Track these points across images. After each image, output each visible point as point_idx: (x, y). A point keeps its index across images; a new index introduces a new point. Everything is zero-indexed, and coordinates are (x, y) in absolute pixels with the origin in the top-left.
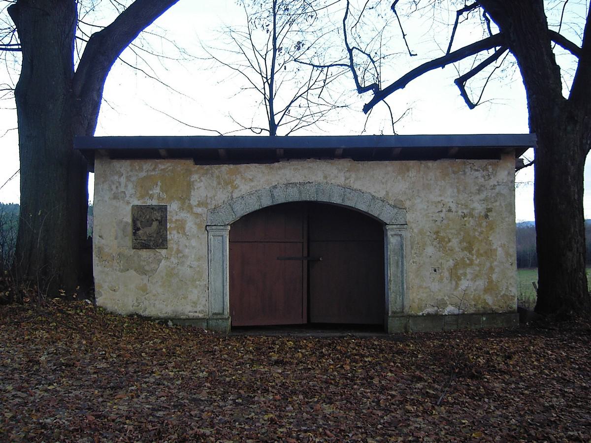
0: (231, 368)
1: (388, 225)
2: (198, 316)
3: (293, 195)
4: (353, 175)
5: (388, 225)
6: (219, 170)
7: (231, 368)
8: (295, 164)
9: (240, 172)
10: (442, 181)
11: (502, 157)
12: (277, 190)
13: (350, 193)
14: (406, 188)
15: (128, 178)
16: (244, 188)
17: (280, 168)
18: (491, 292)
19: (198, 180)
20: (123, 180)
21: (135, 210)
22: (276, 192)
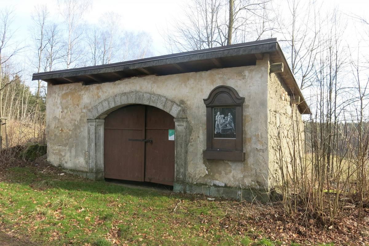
0: (63, 62)
1: (175, 118)
2: (63, 165)
3: (124, 101)
4: (156, 86)
5: (175, 118)
6: (92, 87)
7: (63, 62)
8: (126, 81)
9: (101, 88)
10: (211, 86)
11: (257, 63)
12: (117, 98)
13: (153, 97)
14: (187, 92)
15: (58, 95)
16: (103, 96)
17: (119, 84)
18: (41, 92)
19: (84, 94)
20: (56, 96)
21: (95, 71)
22: (118, 99)
